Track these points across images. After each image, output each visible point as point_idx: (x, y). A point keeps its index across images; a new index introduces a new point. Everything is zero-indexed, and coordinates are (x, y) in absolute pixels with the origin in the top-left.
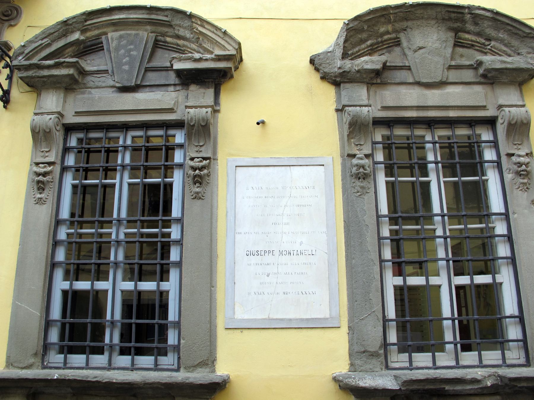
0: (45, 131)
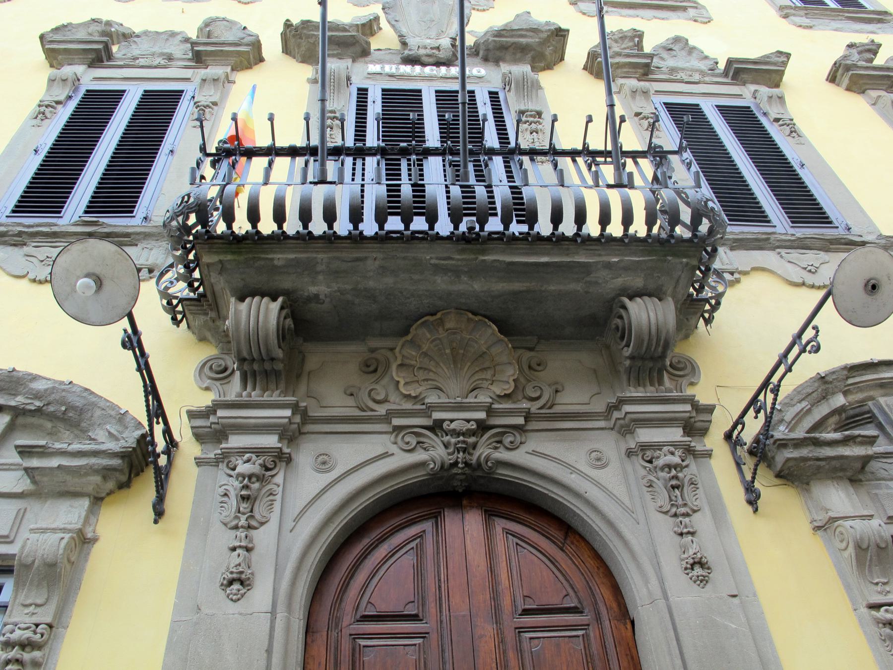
0: (860, 547)
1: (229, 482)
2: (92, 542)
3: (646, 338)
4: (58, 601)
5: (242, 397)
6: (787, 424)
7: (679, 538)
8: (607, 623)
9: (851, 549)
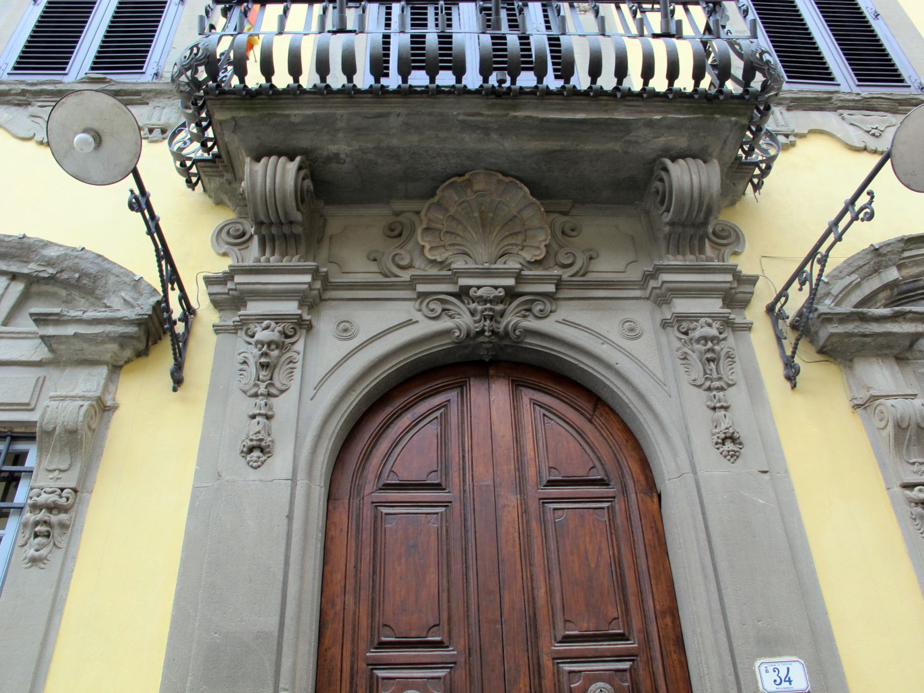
1: (247, 349)
2: (112, 410)
3: (688, 203)
4: (81, 467)
5: (260, 262)
6: (833, 298)
7: (712, 412)
8: (633, 496)
9: (890, 429)
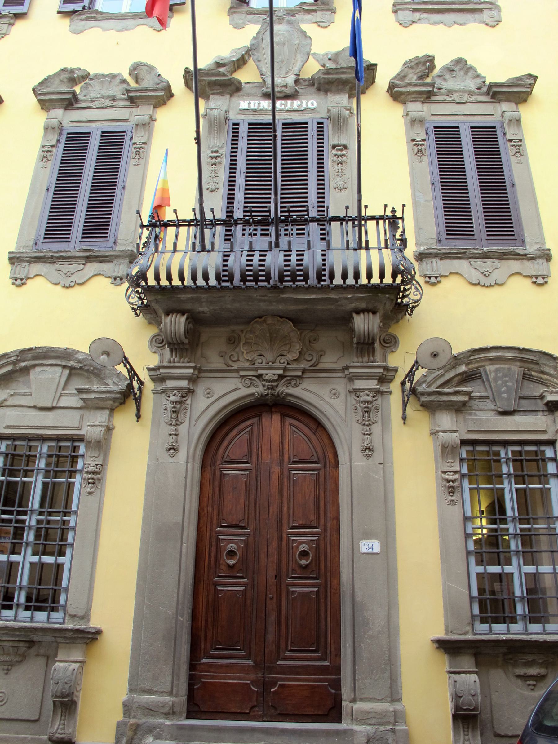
7: (363, 436)
